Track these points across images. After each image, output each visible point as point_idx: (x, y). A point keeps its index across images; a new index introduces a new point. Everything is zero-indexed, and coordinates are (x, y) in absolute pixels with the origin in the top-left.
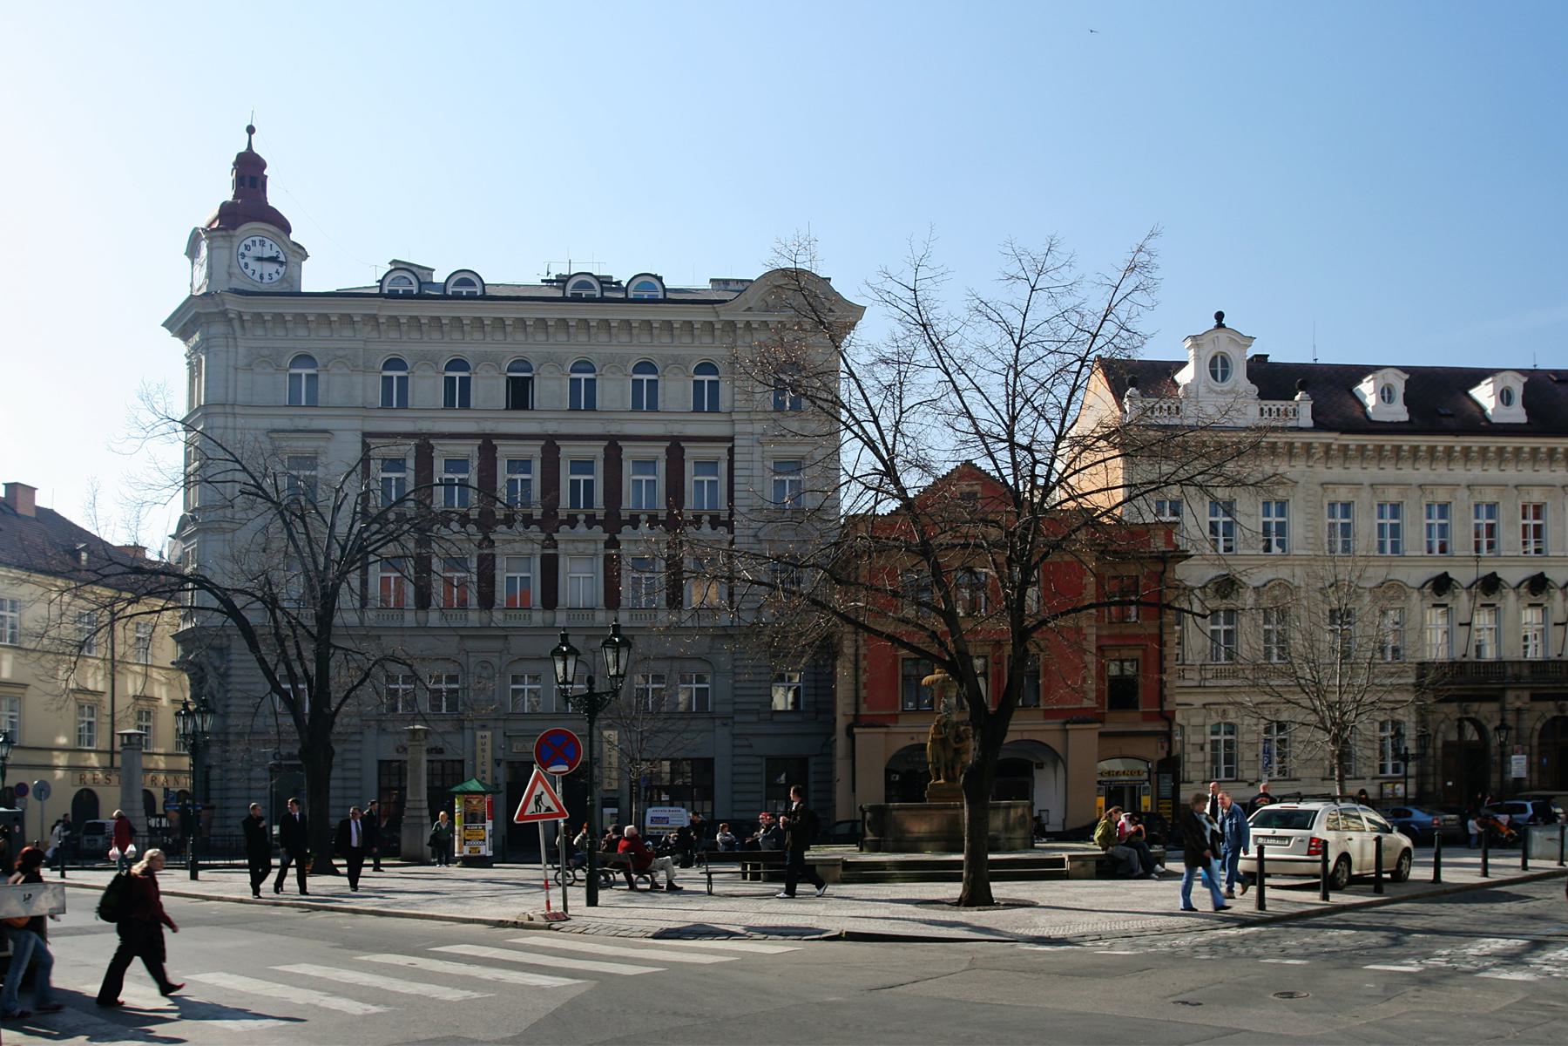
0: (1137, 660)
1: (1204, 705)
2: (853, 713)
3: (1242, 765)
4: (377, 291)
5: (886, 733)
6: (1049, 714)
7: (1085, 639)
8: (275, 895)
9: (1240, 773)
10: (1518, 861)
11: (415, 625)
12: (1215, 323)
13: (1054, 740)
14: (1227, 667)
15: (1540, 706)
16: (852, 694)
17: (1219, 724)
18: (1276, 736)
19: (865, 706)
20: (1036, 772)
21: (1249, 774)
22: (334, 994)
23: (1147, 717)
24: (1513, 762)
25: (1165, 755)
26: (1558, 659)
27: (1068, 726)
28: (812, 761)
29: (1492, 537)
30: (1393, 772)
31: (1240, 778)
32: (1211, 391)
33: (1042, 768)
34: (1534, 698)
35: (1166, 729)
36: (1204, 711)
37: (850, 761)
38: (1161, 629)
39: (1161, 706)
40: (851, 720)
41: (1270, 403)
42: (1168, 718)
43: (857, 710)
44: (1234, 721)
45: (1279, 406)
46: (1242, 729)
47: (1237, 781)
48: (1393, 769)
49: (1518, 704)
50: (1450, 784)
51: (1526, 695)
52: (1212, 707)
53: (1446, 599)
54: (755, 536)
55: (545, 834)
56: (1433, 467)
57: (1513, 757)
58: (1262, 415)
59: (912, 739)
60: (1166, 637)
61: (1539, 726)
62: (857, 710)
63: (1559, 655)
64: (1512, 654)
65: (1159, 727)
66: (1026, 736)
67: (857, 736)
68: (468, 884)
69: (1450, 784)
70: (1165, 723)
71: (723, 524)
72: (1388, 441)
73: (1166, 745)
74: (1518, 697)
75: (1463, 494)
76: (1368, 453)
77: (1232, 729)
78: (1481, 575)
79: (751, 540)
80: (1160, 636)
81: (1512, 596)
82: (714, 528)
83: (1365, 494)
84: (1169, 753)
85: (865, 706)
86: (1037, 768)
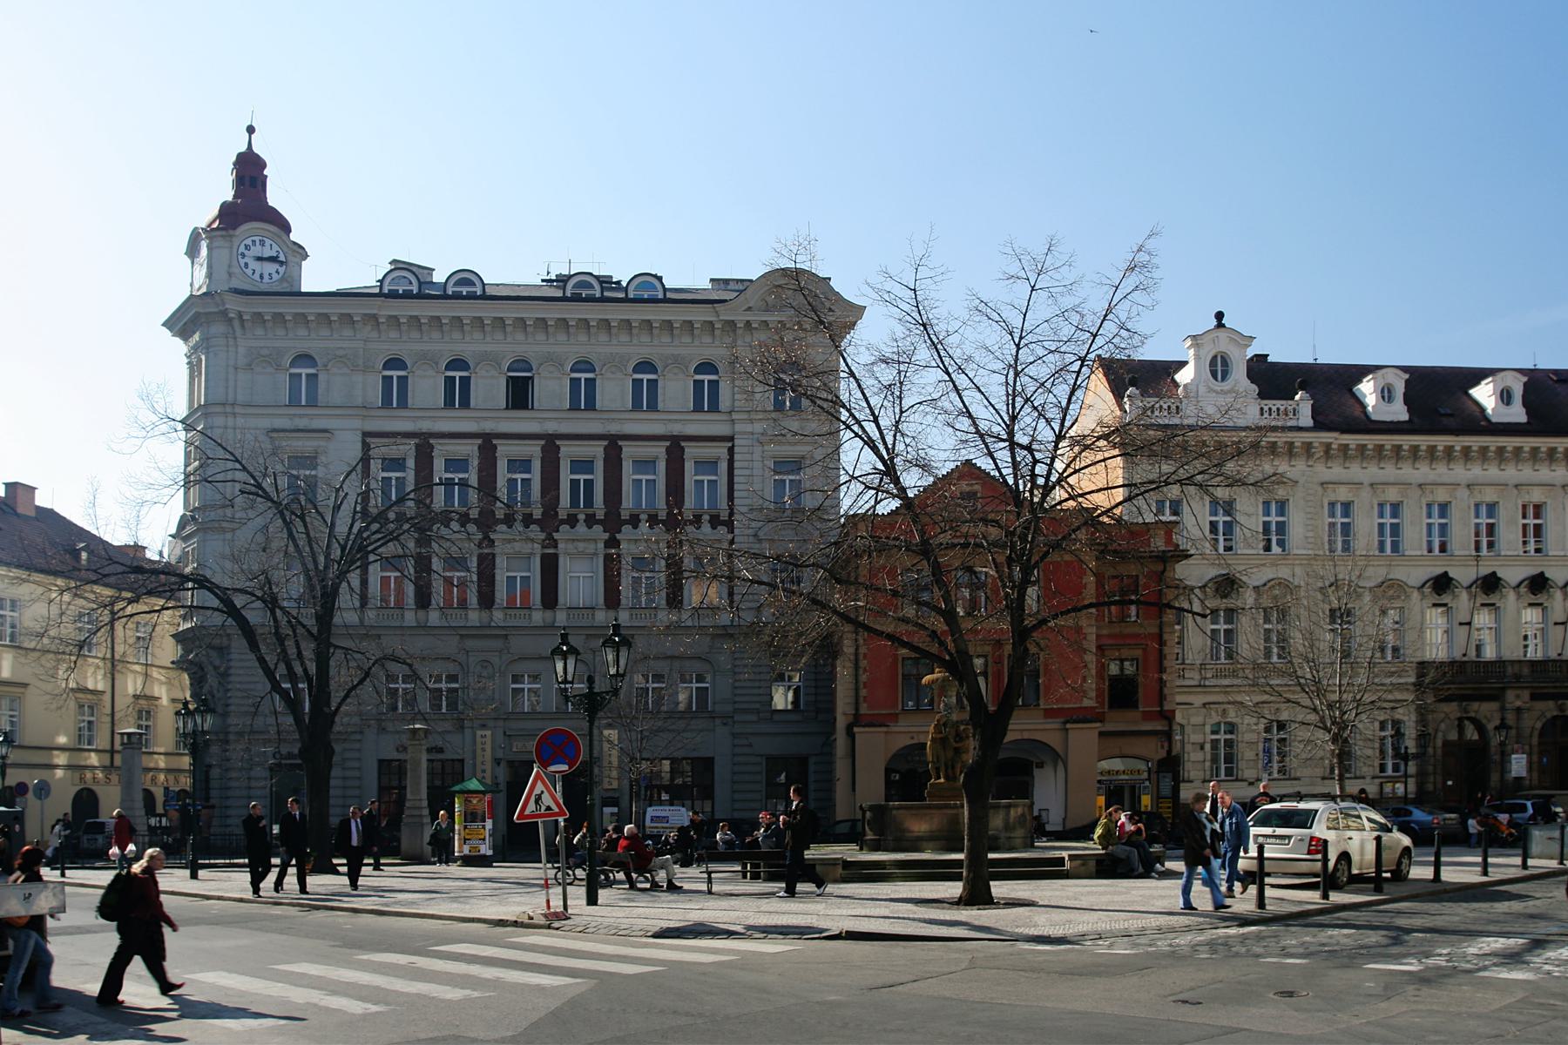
0: (1137, 659)
1: (1204, 704)
2: (853, 712)
3: (1242, 765)
4: (377, 291)
5: (886, 732)
6: (1049, 713)
7: (1085, 638)
8: (275, 895)
9: (1240, 772)
10: (1518, 861)
11: (415, 625)
12: (1215, 322)
13: (1054, 740)
14: (1227, 666)
15: (1540, 705)
16: (852, 693)
17: (1219, 724)
18: (1276, 735)
19: (865, 705)
20: (1036, 772)
21: (1249, 774)
22: (334, 993)
23: (1147, 716)
24: (1513, 762)
25: (1165, 755)
26: (1558, 658)
27: (1068, 726)
28: (812, 760)
29: (1492, 536)
30: (1393, 771)
31: (1240, 777)
32: (1211, 390)
33: (1042, 767)
34: (1534, 697)
35: (1166, 728)
36: (1204, 710)
37: (850, 761)
38: (1161, 629)
39: (1161, 705)
40: (851, 719)
41: (1270, 403)
42: (1168, 717)
43: (857, 709)
44: (1234, 720)
45: (1279, 406)
46: (1242, 728)
47: (1237, 780)
48: (1393, 768)
49: (1518, 703)
50: (1450, 783)
51: (1526, 694)
52: (1212, 706)
53: (1446, 599)
54: (755, 535)
55: (545, 833)
56: (1433, 467)
57: (1513, 756)
58: (1262, 414)
59: (912, 738)
60: (1166, 637)
61: (1539, 725)
62: (857, 709)
63: (1559, 655)
64: (1512, 653)
65: (1159, 726)
66: (1026, 736)
67: (857, 736)
68: (468, 883)
69: (1450, 783)
70: (1165, 722)
71: (723, 523)
72: (1388, 441)
73: (1166, 745)
74: (1518, 697)
75: (1463, 493)
76: (1368, 452)
77: (1232, 728)
78: (1481, 575)
79: (751, 539)
80: (1160, 636)
81: (1512, 596)
82: (714, 527)
83: (1365, 494)
84: (1169, 752)
85: (865, 705)
86: (1037, 767)
